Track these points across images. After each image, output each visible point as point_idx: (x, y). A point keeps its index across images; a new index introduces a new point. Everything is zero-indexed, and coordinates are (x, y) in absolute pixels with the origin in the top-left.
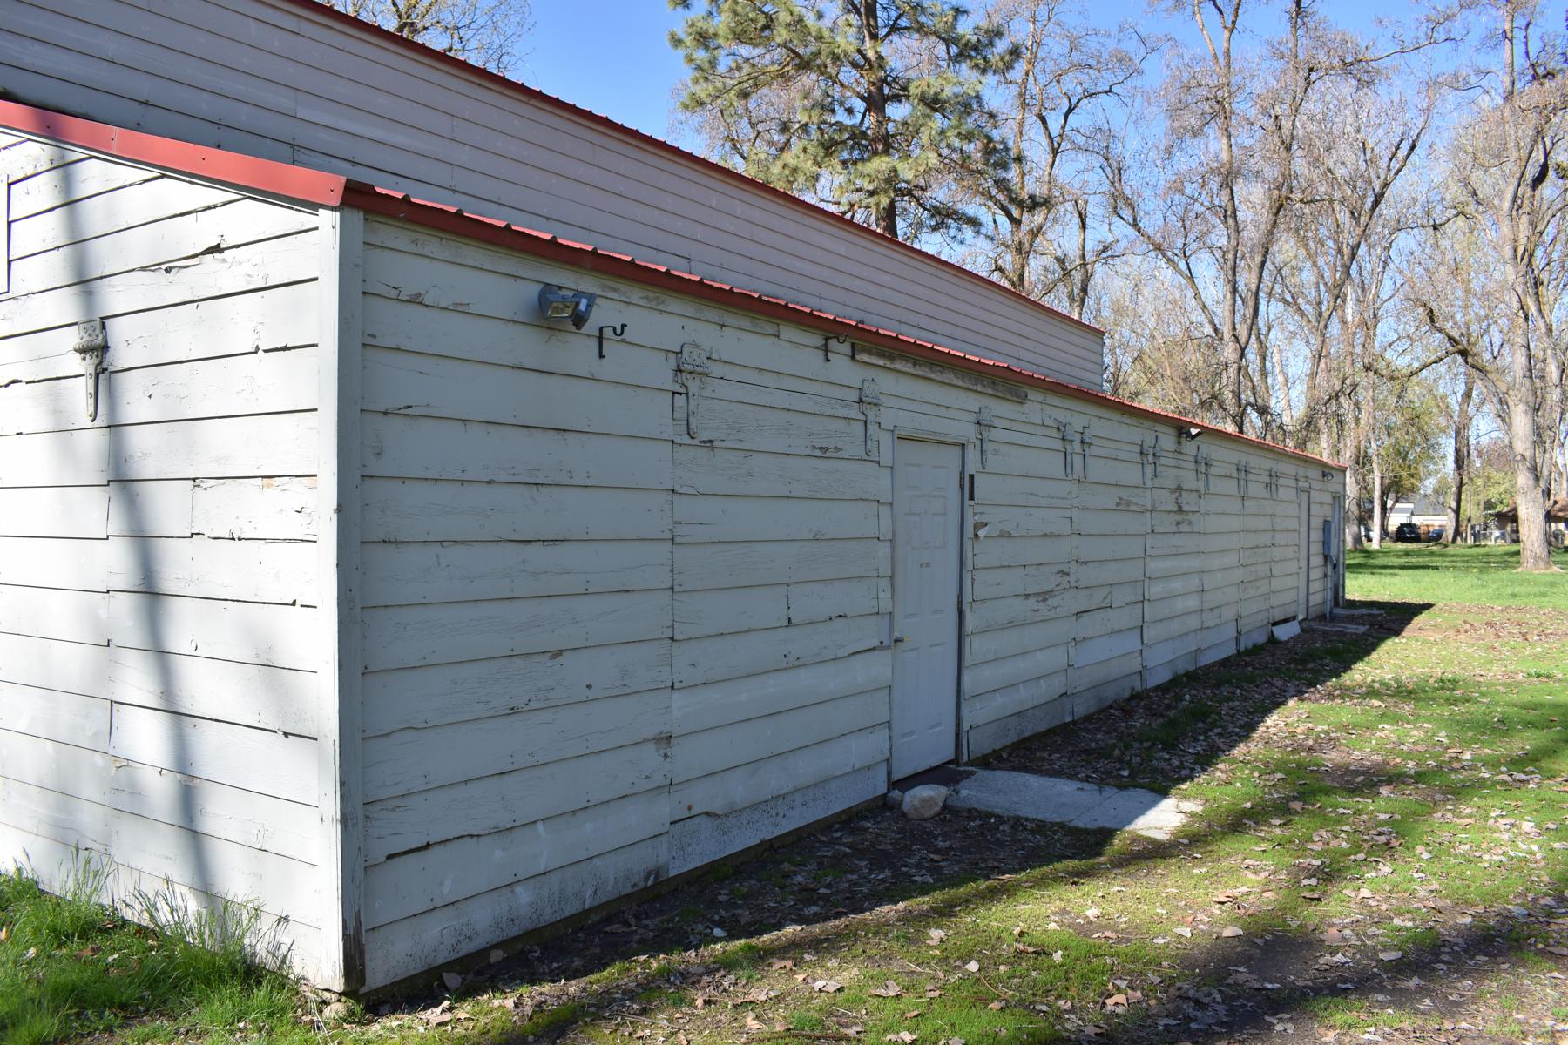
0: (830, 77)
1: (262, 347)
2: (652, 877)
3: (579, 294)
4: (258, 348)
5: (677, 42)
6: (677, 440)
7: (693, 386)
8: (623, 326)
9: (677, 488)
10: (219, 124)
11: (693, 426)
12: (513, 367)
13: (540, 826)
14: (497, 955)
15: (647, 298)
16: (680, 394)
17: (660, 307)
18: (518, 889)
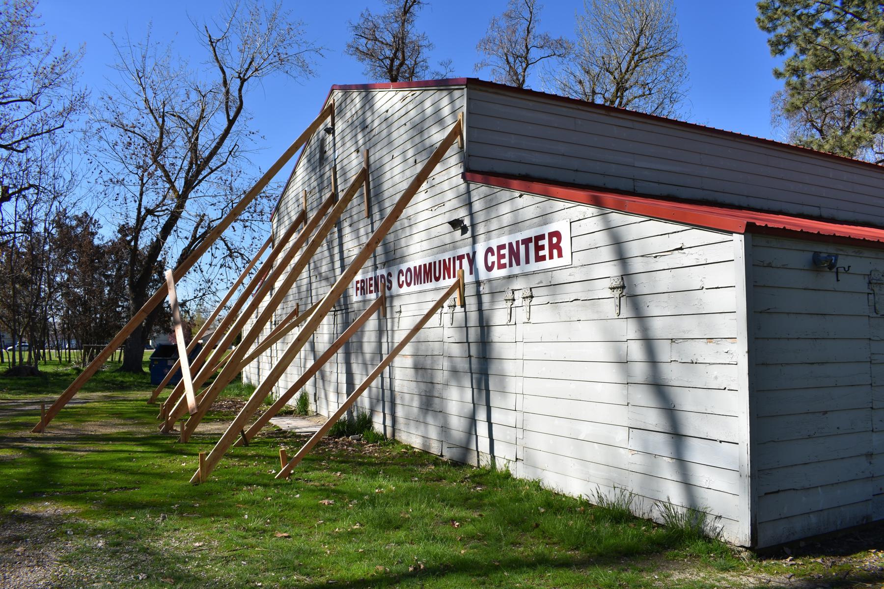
0: (878, 81)
1: (705, 287)
2: (865, 520)
3: (830, 255)
4: (703, 287)
5: (778, 75)
6: (871, 315)
7: (876, 289)
8: (849, 267)
9: (872, 338)
10: (604, 175)
11: (877, 308)
12: (804, 289)
13: (819, 489)
14: (802, 544)
15: (854, 252)
16: (871, 294)
17: (861, 255)
18: (811, 516)
